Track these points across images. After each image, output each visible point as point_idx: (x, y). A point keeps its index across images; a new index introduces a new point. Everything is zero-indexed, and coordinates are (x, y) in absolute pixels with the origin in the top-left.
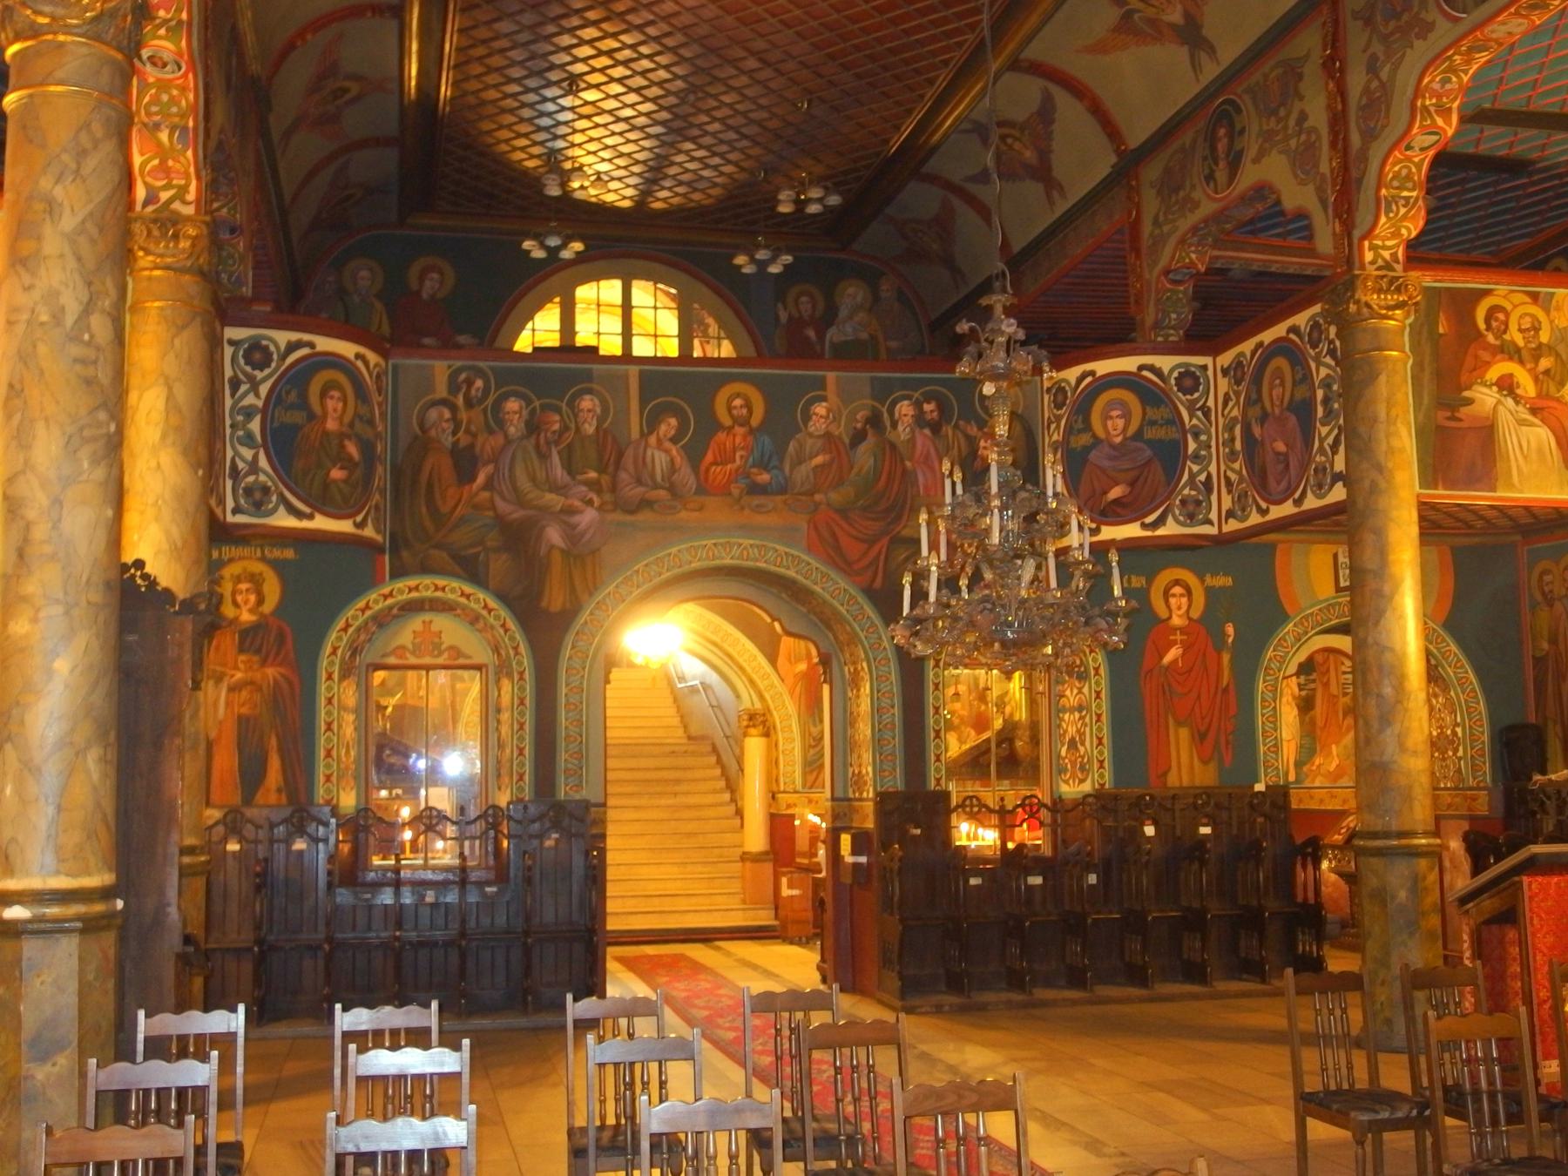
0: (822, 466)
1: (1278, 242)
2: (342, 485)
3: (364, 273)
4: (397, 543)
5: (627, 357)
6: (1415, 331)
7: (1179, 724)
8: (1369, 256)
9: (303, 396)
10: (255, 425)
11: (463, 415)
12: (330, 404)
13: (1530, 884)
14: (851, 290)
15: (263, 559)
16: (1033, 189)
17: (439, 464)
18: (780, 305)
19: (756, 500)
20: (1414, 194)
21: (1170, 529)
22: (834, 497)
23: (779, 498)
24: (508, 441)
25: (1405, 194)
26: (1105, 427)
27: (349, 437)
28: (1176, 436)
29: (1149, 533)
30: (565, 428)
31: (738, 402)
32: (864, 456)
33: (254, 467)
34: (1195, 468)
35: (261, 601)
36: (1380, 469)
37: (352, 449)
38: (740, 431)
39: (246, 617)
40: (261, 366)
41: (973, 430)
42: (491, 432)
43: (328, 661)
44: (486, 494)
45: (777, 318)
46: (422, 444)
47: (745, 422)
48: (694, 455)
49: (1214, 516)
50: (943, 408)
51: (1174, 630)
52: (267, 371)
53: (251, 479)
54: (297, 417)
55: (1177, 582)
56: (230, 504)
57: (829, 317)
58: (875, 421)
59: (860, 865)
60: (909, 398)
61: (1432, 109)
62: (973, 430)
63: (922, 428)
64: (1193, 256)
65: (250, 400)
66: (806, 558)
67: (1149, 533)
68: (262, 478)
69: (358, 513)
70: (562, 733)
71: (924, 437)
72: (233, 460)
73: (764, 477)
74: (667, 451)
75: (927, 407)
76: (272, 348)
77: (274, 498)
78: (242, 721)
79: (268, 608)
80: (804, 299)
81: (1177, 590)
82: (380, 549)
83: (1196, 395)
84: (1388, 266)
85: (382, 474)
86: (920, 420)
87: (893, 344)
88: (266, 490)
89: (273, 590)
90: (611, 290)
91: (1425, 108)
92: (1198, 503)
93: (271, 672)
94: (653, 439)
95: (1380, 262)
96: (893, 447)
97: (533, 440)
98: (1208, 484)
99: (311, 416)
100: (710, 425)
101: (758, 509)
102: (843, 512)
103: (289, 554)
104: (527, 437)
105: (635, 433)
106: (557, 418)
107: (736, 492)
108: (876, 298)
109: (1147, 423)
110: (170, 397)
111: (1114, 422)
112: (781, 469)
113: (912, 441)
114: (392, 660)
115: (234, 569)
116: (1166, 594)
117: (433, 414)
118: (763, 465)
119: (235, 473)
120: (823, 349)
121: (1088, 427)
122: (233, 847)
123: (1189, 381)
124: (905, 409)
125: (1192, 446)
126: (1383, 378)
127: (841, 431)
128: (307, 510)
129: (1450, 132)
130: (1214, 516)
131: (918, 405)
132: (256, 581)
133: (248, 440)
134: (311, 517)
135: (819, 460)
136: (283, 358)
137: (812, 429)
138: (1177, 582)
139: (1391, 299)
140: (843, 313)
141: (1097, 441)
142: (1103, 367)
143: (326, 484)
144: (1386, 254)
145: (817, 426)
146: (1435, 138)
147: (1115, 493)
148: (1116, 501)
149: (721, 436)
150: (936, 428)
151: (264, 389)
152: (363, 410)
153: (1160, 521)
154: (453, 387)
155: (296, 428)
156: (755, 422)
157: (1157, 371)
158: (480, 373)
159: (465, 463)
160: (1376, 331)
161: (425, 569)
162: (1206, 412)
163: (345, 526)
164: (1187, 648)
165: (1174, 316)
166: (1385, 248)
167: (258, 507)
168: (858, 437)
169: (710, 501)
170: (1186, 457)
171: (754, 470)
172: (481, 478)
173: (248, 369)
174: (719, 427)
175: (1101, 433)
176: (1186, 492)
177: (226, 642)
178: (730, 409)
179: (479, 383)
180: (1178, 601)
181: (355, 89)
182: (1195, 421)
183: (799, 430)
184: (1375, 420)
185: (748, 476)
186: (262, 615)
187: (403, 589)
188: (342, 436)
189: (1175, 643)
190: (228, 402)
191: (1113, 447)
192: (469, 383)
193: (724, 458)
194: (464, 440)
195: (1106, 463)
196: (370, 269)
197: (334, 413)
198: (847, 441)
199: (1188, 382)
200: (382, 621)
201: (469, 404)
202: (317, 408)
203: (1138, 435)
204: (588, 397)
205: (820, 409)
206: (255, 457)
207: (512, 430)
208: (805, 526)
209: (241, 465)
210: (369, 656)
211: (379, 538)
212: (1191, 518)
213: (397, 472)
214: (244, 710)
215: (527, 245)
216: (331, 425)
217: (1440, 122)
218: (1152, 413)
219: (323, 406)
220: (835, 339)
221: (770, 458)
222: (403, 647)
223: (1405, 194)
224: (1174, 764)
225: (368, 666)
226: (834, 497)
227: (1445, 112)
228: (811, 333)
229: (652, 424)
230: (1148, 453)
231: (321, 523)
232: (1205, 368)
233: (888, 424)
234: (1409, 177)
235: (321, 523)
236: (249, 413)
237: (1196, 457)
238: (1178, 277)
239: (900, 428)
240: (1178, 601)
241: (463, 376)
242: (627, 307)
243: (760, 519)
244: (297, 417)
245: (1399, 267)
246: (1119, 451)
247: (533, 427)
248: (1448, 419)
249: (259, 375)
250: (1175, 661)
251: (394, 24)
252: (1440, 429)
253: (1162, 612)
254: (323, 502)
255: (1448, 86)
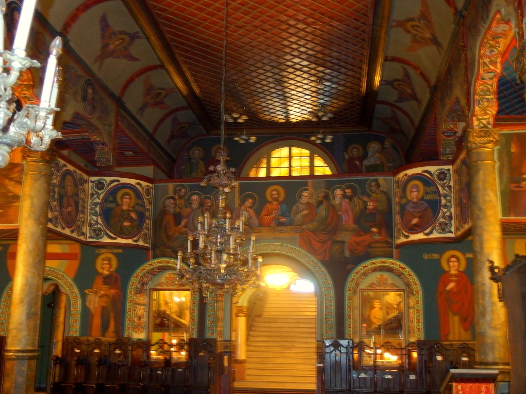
0: (305, 215)
1: (519, 116)
2: (128, 227)
3: (197, 152)
4: (154, 247)
5: (312, 176)
6: (500, 152)
7: (454, 314)
8: (476, 123)
9: (115, 198)
10: (98, 209)
11: (178, 202)
12: (125, 200)
13: (457, 386)
14: (373, 145)
15: (112, 253)
16: (413, 103)
17: (169, 219)
18: (345, 153)
19: (282, 228)
20: (491, 97)
21: (435, 235)
22: (310, 226)
23: (288, 227)
24: (193, 210)
25: (487, 97)
26: (410, 195)
27: (131, 211)
28: (438, 198)
29: (426, 237)
30: (213, 205)
31: (274, 192)
32: (322, 211)
33: (97, 223)
34: (445, 210)
35: (110, 267)
36: (480, 209)
37: (133, 215)
38: (275, 203)
39: (106, 273)
40: (100, 189)
41: (366, 199)
42: (187, 207)
43: (131, 288)
44: (184, 229)
45: (344, 158)
46: (164, 213)
47: (276, 200)
48: (258, 212)
49: (453, 229)
50: (354, 192)
51: (452, 276)
52: (102, 190)
53: (95, 227)
54: (112, 205)
55: (453, 256)
56: (88, 235)
57: (365, 155)
58: (326, 197)
59: (320, 367)
60: (340, 188)
61: (487, 63)
62: (366, 199)
63: (345, 198)
64: (451, 126)
65: (97, 200)
66: (298, 249)
67: (135, 243)
68: (99, 226)
69: (135, 237)
70: (208, 314)
71: (346, 203)
72: (90, 220)
73: (283, 220)
74: (247, 211)
75: (347, 191)
76: (105, 183)
77: (103, 233)
78: (103, 308)
79: (113, 269)
80: (355, 150)
81: (453, 259)
82: (147, 249)
83: (445, 181)
84: (485, 126)
85: (148, 223)
86: (344, 196)
87: (390, 165)
88: (100, 230)
89: (114, 263)
90: (284, 151)
91: (485, 63)
92: (446, 224)
93: (113, 291)
94: (243, 208)
95: (482, 125)
96: (333, 206)
97: (200, 210)
98: (450, 217)
99: (118, 205)
100: (264, 201)
101: (281, 232)
102: (313, 232)
103: (120, 251)
104: (199, 209)
105: (237, 205)
106: (209, 201)
107: (273, 225)
108: (383, 148)
109: (427, 193)
110: (32, 203)
111: (414, 194)
112: (289, 216)
113: (341, 204)
114: (159, 287)
115: (103, 256)
116: (448, 261)
117: (168, 202)
118: (283, 215)
119: (91, 225)
120: (362, 169)
121: (406, 197)
122: (97, 351)
123: (442, 176)
124: (338, 192)
125: (443, 201)
126: (481, 172)
127: (313, 201)
128: (114, 236)
129: (498, 71)
130: (453, 229)
131: (344, 190)
132: (109, 260)
133: (95, 214)
134: (115, 239)
135: (305, 212)
136: (109, 185)
137: (302, 201)
138: (453, 256)
139: (485, 139)
140: (370, 154)
141: (409, 201)
142: (411, 172)
143: (122, 228)
144: (484, 122)
145: (304, 200)
146: (492, 74)
147: (415, 221)
148: (415, 225)
149: (268, 205)
150: (350, 198)
151: (101, 196)
152: (139, 202)
153: (431, 232)
154: (175, 192)
155: (111, 209)
156: (281, 199)
157: (429, 172)
158: (184, 187)
159: (178, 218)
160: (479, 153)
161: (164, 256)
162: (449, 187)
163: (130, 241)
164: (458, 283)
165: (448, 149)
166: (484, 119)
167: (98, 236)
168: (320, 203)
169: (264, 229)
170: (441, 206)
171: (280, 217)
172: (183, 223)
173: (97, 190)
174: (267, 201)
175: (409, 198)
176: (441, 220)
177: (99, 281)
178: (271, 195)
179: (183, 190)
180: (454, 264)
181: (164, 93)
182: (444, 192)
183: (297, 202)
184: (478, 189)
185: (277, 219)
186: (110, 272)
187: (156, 263)
188: (129, 211)
189: (451, 281)
190: (90, 201)
191: (414, 203)
192: (180, 190)
193: (269, 213)
194: (178, 210)
195: (411, 210)
196: (199, 150)
197: (126, 203)
198: (315, 205)
199: (442, 176)
200: (153, 273)
201: (180, 198)
202: (119, 201)
203: (422, 199)
204: (338, 189)
205: (305, 194)
206: (97, 219)
207: (194, 206)
208: (298, 238)
209: (92, 222)
210: (150, 285)
211: (147, 245)
212: (443, 230)
213: (155, 223)
214: (104, 304)
215: (236, 139)
216: (125, 207)
217: (492, 67)
218: (429, 189)
219: (122, 201)
220: (367, 164)
221: (285, 213)
222: (162, 283)
223: (487, 97)
224: (451, 330)
225: (150, 289)
226: (310, 226)
227: (494, 63)
228: (357, 163)
229: (243, 201)
230: (426, 205)
231: (120, 240)
232: (449, 170)
233: (331, 198)
234: (488, 90)
235: (120, 240)
236: (96, 204)
237: (445, 206)
238: (448, 134)
239: (336, 199)
240: (454, 264)
241: (178, 188)
242: (290, 157)
243: (282, 235)
244: (112, 205)
245: (490, 127)
246: (416, 205)
247: (201, 205)
248: (516, 187)
249: (100, 192)
250: (452, 289)
251: (163, 71)
252: (512, 192)
253: (446, 268)
254: (121, 233)
255: (494, 53)
